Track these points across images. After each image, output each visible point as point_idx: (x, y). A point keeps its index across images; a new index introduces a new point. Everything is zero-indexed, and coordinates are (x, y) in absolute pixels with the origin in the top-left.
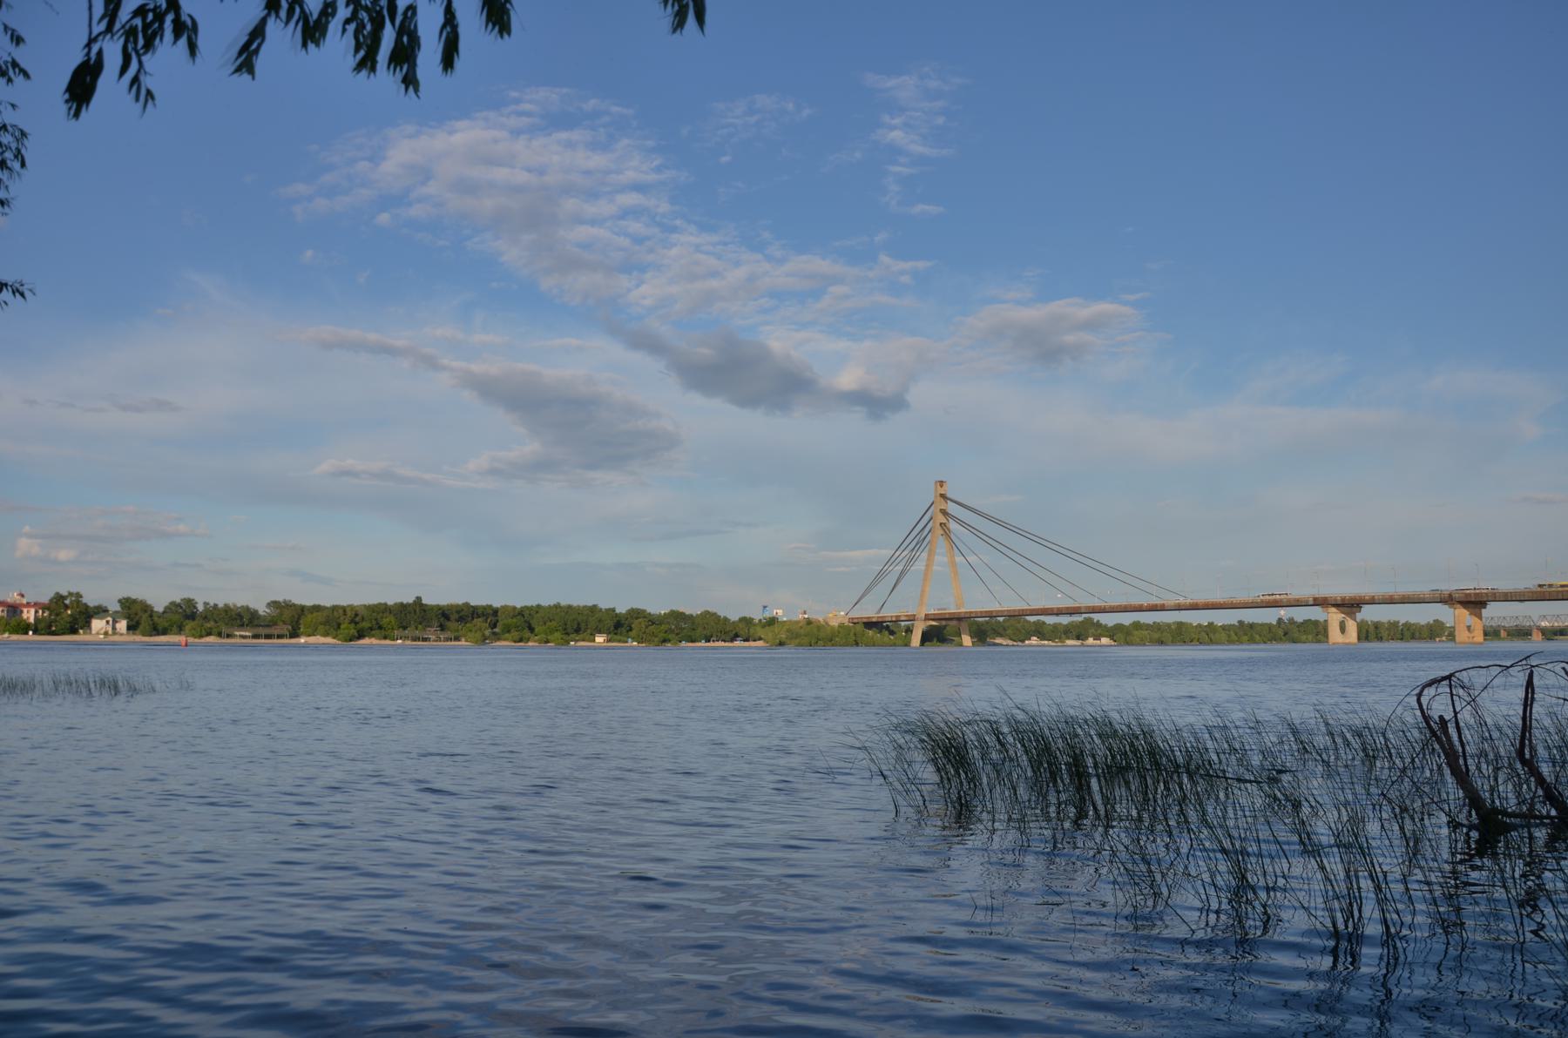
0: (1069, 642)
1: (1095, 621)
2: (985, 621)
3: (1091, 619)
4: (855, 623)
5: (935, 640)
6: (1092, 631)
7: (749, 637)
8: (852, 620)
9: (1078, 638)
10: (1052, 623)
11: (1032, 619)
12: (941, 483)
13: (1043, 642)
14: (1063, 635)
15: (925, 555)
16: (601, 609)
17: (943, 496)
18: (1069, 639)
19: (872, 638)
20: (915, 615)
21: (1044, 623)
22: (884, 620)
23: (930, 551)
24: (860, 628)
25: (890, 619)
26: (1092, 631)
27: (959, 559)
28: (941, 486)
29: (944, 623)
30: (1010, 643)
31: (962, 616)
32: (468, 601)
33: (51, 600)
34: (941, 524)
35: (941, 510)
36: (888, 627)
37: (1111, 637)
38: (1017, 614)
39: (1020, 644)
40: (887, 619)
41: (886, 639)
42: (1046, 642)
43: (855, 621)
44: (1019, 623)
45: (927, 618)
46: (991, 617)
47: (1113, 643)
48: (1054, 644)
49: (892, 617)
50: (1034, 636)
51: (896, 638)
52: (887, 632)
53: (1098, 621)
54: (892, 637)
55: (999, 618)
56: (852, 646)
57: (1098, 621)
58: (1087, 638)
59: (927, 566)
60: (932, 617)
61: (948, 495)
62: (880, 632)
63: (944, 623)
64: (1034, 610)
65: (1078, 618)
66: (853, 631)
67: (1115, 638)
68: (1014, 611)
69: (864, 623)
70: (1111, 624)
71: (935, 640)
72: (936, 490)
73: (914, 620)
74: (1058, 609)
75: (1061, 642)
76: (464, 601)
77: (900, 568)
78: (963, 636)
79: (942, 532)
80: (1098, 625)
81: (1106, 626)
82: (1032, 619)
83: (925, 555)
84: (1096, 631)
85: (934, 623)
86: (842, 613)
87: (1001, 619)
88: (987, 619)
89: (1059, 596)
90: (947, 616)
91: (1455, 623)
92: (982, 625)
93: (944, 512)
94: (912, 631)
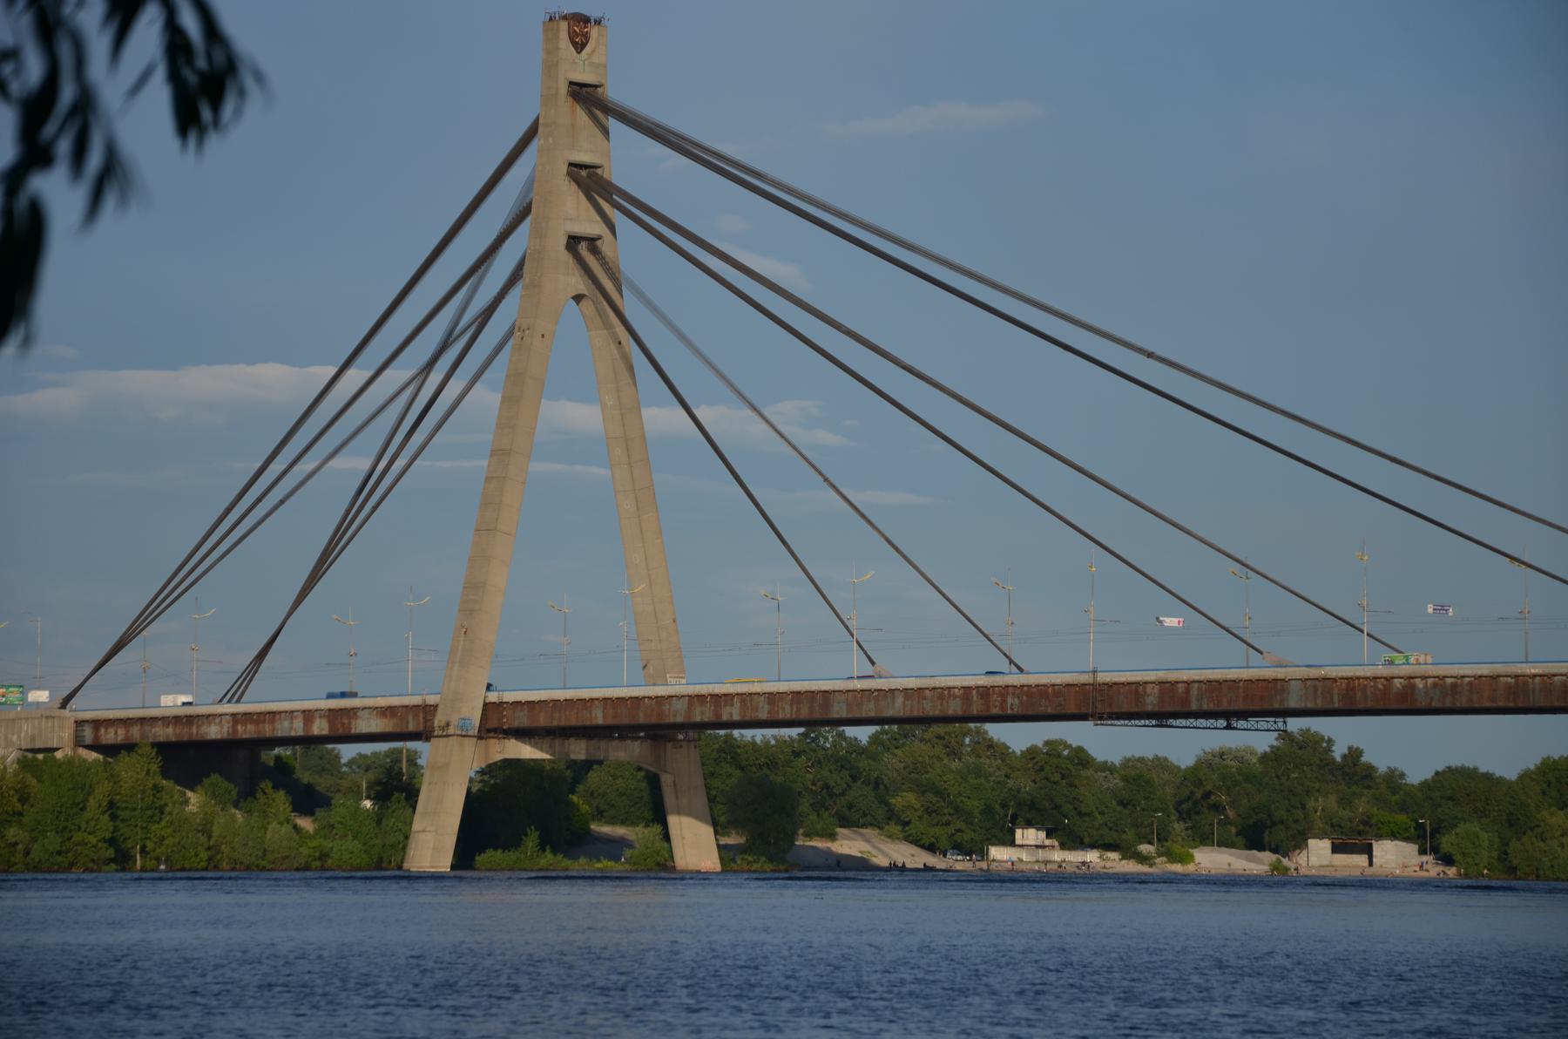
0: (1210, 860)
1: (1338, 752)
2: (781, 743)
3: (1315, 745)
4: (110, 750)
5: (532, 840)
6: (1323, 803)
7: (326, 802)
8: (91, 733)
9: (1253, 839)
10: (1115, 758)
11: (1019, 737)
12: (580, 28)
13: (1074, 857)
14: (1178, 827)
15: (487, 398)
16: (1370, 768)
17: (585, 95)
18: (1205, 840)
19: (206, 830)
20: (428, 710)
21: (1081, 758)
22: (267, 731)
23: (516, 377)
24: (133, 772)
25: (298, 728)
26: (1323, 803)
27: (662, 417)
28: (579, 47)
29: (578, 750)
30: (913, 857)
31: (677, 714)
32: (1168, 756)
33: (1525, 776)
34: (573, 241)
35: (575, 166)
36: (282, 768)
37: (1427, 840)
38: (954, 708)
39: (960, 863)
40: (283, 729)
41: (277, 833)
42: (1092, 856)
43: (111, 736)
44: (954, 754)
45: (495, 723)
46: (809, 724)
47: (1434, 870)
48: (1131, 867)
49: (308, 715)
50: (1029, 824)
51: (328, 829)
52: (281, 800)
53: (1354, 754)
54: (305, 823)
55: (850, 731)
56: (94, 866)
57: (1354, 754)
58: (1299, 842)
59: (500, 454)
60: (522, 720)
61: (614, 93)
62: (247, 793)
63: (578, 750)
64: (1041, 691)
65: (1257, 739)
66: (102, 790)
67: (1447, 842)
68: (943, 693)
69: (163, 748)
70: (1417, 772)
71: (532, 840)
72: (550, 67)
73: (424, 735)
74: (1167, 687)
75: (1173, 858)
76: (1029, 745)
77: (355, 463)
78: (673, 820)
79: (578, 284)
80: (1354, 770)
81: (1393, 779)
82: (1019, 737)
83: (487, 398)
84: (1345, 802)
85: (526, 751)
86: (41, 696)
87: (863, 734)
88: (794, 732)
89: (1171, 622)
90: (598, 717)
91: (1021, 846)
92: (772, 764)
93: (589, 180)
94: (411, 794)
